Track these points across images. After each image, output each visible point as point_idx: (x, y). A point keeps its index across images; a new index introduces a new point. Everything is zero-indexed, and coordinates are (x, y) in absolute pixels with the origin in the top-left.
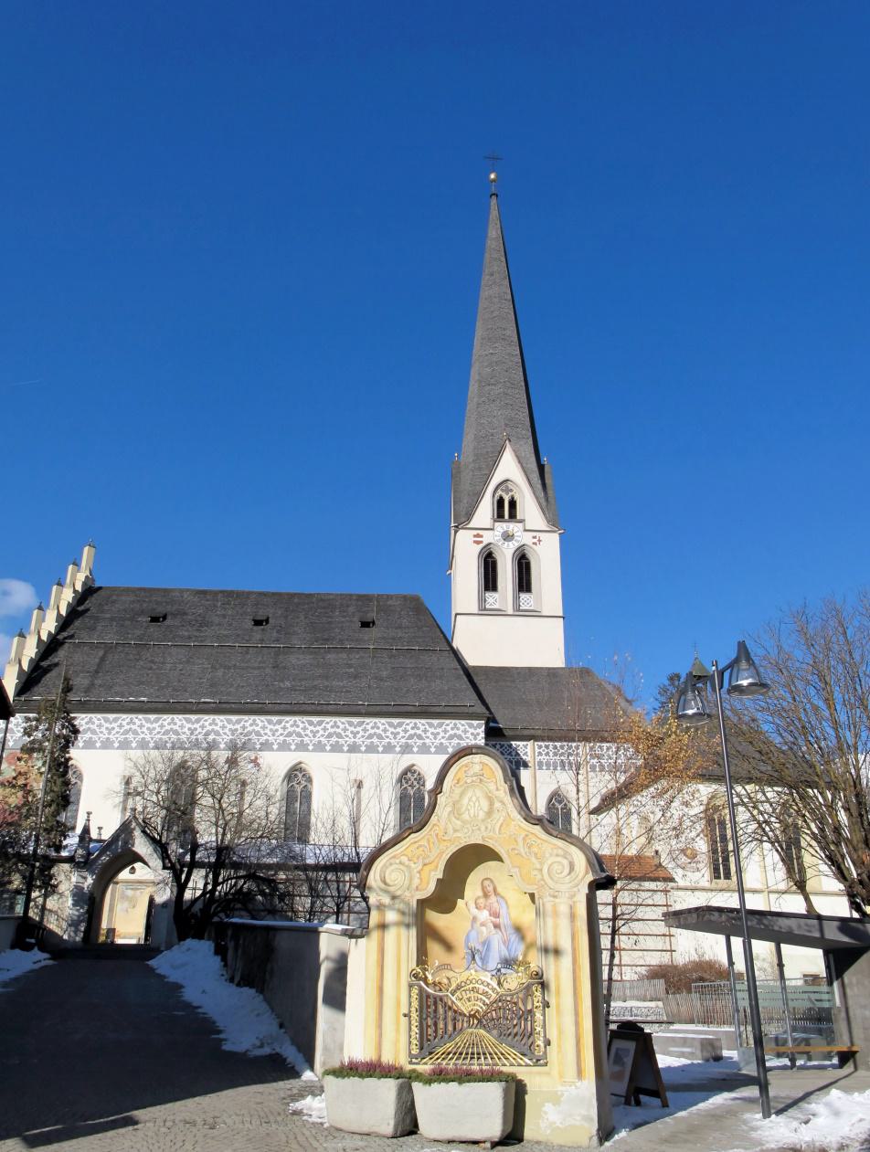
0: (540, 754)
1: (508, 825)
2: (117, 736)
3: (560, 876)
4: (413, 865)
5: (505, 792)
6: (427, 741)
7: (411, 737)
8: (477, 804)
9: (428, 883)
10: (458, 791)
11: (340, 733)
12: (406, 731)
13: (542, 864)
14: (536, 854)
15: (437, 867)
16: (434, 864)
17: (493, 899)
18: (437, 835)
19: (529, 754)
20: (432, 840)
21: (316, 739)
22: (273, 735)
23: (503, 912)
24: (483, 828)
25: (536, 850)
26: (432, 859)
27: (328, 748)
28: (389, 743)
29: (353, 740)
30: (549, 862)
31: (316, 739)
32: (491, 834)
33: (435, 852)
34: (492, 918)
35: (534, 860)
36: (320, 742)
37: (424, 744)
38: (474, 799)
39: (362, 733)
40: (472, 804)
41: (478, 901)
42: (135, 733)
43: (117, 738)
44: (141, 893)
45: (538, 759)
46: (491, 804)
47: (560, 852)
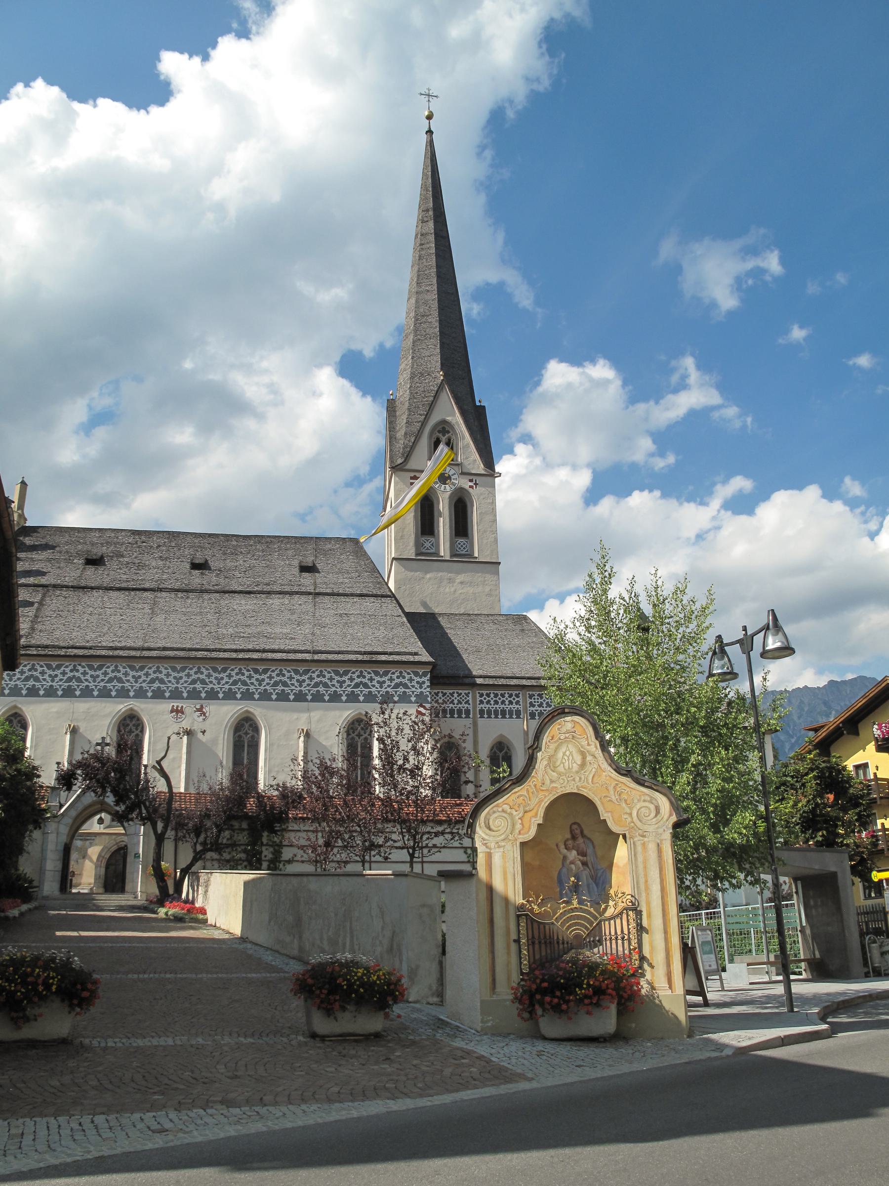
0: (481, 702)
1: (600, 776)
2: (60, 683)
3: (647, 818)
4: (515, 813)
5: (596, 747)
6: (373, 689)
7: (357, 686)
8: (571, 758)
9: (530, 828)
10: (553, 746)
11: (49, 669)
12: (351, 679)
13: (631, 809)
14: (626, 801)
15: (536, 814)
16: (535, 811)
17: (580, 840)
18: (535, 786)
19: (470, 702)
20: (531, 791)
21: (138, 685)
22: (219, 683)
23: (590, 851)
24: (577, 779)
25: (624, 796)
26: (532, 807)
27: (274, 697)
28: (335, 691)
29: (299, 688)
30: (638, 806)
31: (262, 687)
32: (585, 783)
33: (534, 801)
34: (580, 857)
35: (624, 805)
36: (266, 690)
37: (370, 692)
38: (568, 753)
39: (307, 682)
40: (566, 758)
41: (567, 843)
42: (79, 680)
43: (60, 686)
44: (91, 843)
45: (479, 707)
46: (584, 758)
47: (647, 798)
